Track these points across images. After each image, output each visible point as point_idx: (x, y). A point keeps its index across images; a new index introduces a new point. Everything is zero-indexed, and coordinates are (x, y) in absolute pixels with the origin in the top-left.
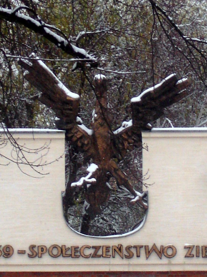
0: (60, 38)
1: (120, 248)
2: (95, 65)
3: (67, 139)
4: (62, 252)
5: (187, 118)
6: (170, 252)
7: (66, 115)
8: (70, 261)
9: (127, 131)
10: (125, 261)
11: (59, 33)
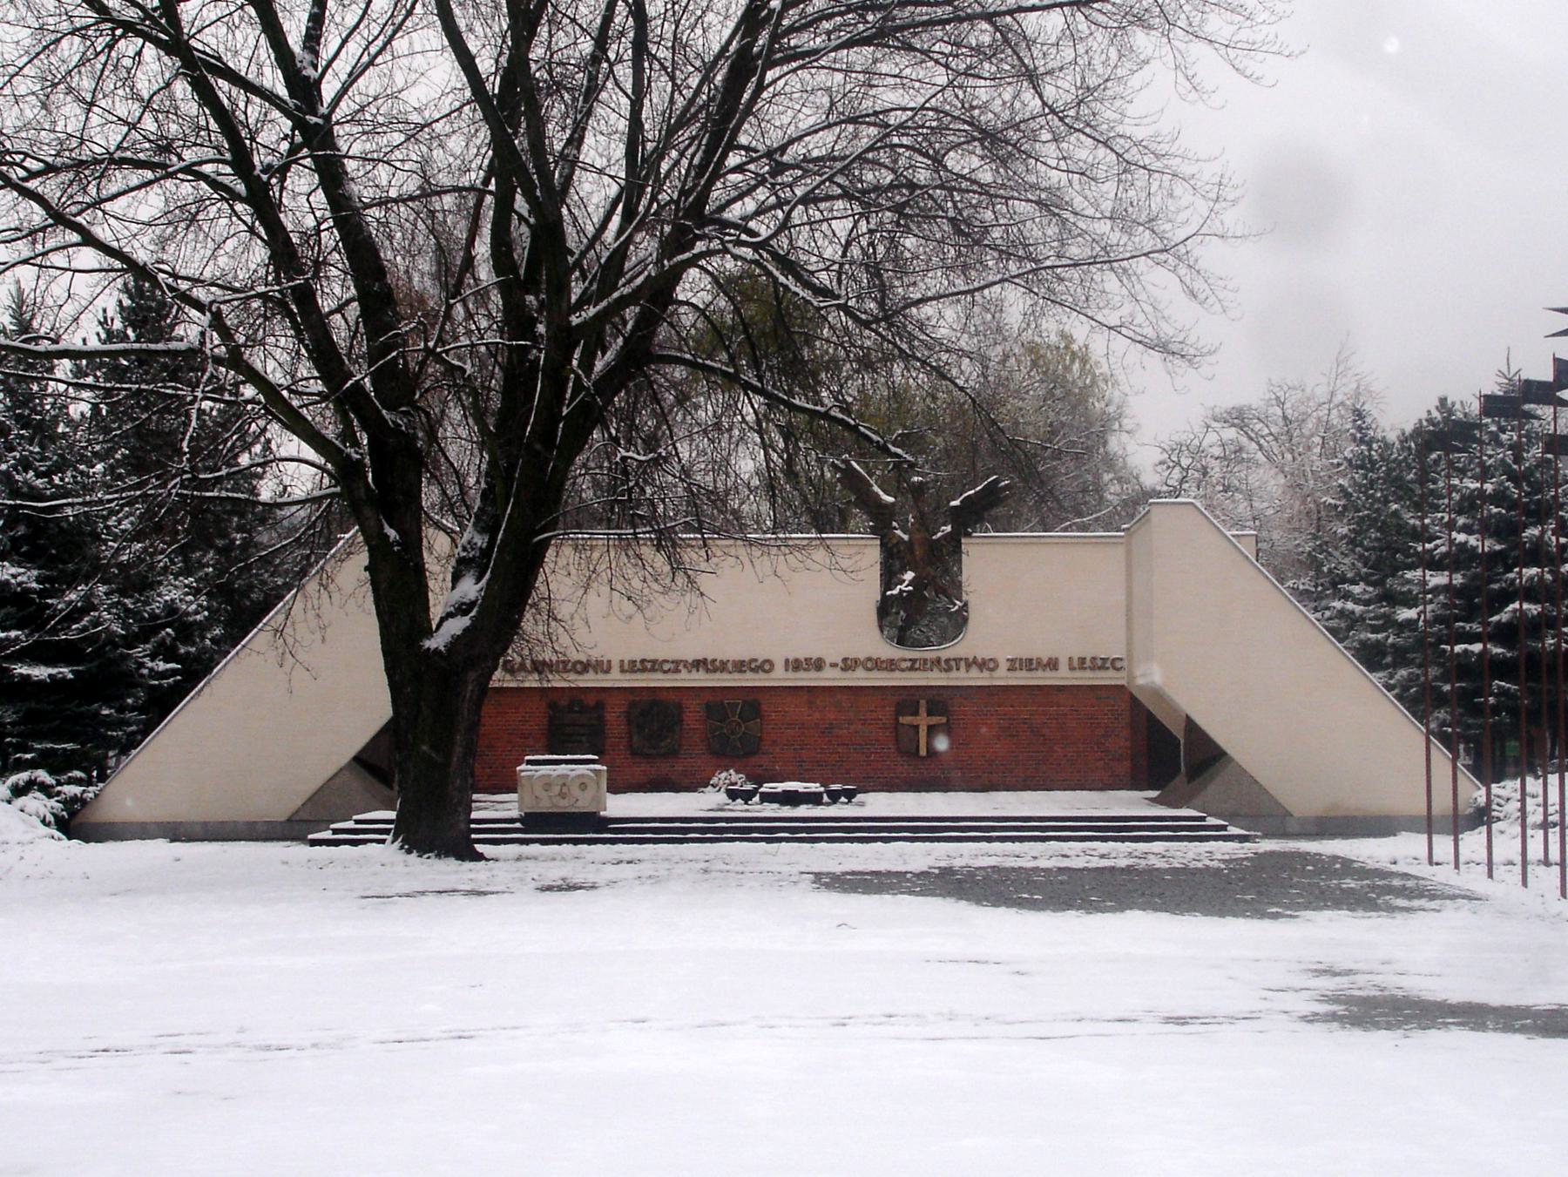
0: (875, 437)
1: (938, 660)
2: (912, 465)
3: (882, 545)
4: (877, 664)
5: (1009, 523)
6: (992, 665)
7: (881, 519)
8: (884, 674)
9: (944, 537)
10: (943, 675)
11: (875, 432)
